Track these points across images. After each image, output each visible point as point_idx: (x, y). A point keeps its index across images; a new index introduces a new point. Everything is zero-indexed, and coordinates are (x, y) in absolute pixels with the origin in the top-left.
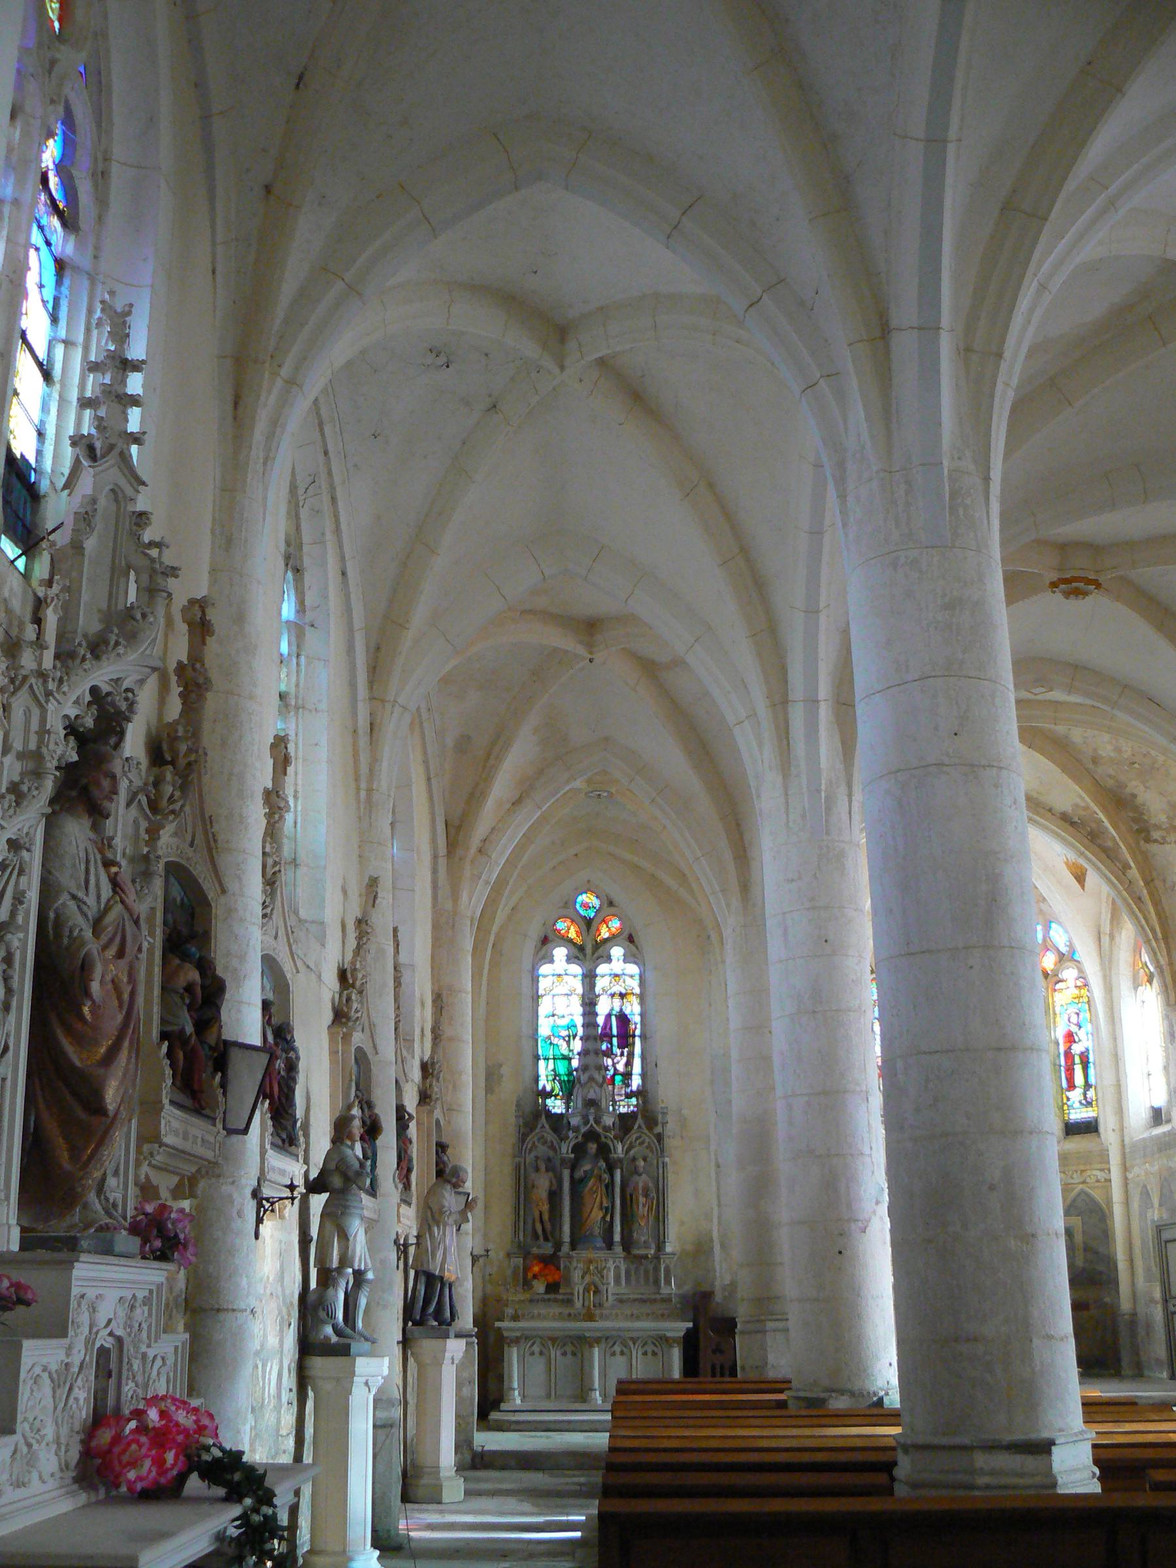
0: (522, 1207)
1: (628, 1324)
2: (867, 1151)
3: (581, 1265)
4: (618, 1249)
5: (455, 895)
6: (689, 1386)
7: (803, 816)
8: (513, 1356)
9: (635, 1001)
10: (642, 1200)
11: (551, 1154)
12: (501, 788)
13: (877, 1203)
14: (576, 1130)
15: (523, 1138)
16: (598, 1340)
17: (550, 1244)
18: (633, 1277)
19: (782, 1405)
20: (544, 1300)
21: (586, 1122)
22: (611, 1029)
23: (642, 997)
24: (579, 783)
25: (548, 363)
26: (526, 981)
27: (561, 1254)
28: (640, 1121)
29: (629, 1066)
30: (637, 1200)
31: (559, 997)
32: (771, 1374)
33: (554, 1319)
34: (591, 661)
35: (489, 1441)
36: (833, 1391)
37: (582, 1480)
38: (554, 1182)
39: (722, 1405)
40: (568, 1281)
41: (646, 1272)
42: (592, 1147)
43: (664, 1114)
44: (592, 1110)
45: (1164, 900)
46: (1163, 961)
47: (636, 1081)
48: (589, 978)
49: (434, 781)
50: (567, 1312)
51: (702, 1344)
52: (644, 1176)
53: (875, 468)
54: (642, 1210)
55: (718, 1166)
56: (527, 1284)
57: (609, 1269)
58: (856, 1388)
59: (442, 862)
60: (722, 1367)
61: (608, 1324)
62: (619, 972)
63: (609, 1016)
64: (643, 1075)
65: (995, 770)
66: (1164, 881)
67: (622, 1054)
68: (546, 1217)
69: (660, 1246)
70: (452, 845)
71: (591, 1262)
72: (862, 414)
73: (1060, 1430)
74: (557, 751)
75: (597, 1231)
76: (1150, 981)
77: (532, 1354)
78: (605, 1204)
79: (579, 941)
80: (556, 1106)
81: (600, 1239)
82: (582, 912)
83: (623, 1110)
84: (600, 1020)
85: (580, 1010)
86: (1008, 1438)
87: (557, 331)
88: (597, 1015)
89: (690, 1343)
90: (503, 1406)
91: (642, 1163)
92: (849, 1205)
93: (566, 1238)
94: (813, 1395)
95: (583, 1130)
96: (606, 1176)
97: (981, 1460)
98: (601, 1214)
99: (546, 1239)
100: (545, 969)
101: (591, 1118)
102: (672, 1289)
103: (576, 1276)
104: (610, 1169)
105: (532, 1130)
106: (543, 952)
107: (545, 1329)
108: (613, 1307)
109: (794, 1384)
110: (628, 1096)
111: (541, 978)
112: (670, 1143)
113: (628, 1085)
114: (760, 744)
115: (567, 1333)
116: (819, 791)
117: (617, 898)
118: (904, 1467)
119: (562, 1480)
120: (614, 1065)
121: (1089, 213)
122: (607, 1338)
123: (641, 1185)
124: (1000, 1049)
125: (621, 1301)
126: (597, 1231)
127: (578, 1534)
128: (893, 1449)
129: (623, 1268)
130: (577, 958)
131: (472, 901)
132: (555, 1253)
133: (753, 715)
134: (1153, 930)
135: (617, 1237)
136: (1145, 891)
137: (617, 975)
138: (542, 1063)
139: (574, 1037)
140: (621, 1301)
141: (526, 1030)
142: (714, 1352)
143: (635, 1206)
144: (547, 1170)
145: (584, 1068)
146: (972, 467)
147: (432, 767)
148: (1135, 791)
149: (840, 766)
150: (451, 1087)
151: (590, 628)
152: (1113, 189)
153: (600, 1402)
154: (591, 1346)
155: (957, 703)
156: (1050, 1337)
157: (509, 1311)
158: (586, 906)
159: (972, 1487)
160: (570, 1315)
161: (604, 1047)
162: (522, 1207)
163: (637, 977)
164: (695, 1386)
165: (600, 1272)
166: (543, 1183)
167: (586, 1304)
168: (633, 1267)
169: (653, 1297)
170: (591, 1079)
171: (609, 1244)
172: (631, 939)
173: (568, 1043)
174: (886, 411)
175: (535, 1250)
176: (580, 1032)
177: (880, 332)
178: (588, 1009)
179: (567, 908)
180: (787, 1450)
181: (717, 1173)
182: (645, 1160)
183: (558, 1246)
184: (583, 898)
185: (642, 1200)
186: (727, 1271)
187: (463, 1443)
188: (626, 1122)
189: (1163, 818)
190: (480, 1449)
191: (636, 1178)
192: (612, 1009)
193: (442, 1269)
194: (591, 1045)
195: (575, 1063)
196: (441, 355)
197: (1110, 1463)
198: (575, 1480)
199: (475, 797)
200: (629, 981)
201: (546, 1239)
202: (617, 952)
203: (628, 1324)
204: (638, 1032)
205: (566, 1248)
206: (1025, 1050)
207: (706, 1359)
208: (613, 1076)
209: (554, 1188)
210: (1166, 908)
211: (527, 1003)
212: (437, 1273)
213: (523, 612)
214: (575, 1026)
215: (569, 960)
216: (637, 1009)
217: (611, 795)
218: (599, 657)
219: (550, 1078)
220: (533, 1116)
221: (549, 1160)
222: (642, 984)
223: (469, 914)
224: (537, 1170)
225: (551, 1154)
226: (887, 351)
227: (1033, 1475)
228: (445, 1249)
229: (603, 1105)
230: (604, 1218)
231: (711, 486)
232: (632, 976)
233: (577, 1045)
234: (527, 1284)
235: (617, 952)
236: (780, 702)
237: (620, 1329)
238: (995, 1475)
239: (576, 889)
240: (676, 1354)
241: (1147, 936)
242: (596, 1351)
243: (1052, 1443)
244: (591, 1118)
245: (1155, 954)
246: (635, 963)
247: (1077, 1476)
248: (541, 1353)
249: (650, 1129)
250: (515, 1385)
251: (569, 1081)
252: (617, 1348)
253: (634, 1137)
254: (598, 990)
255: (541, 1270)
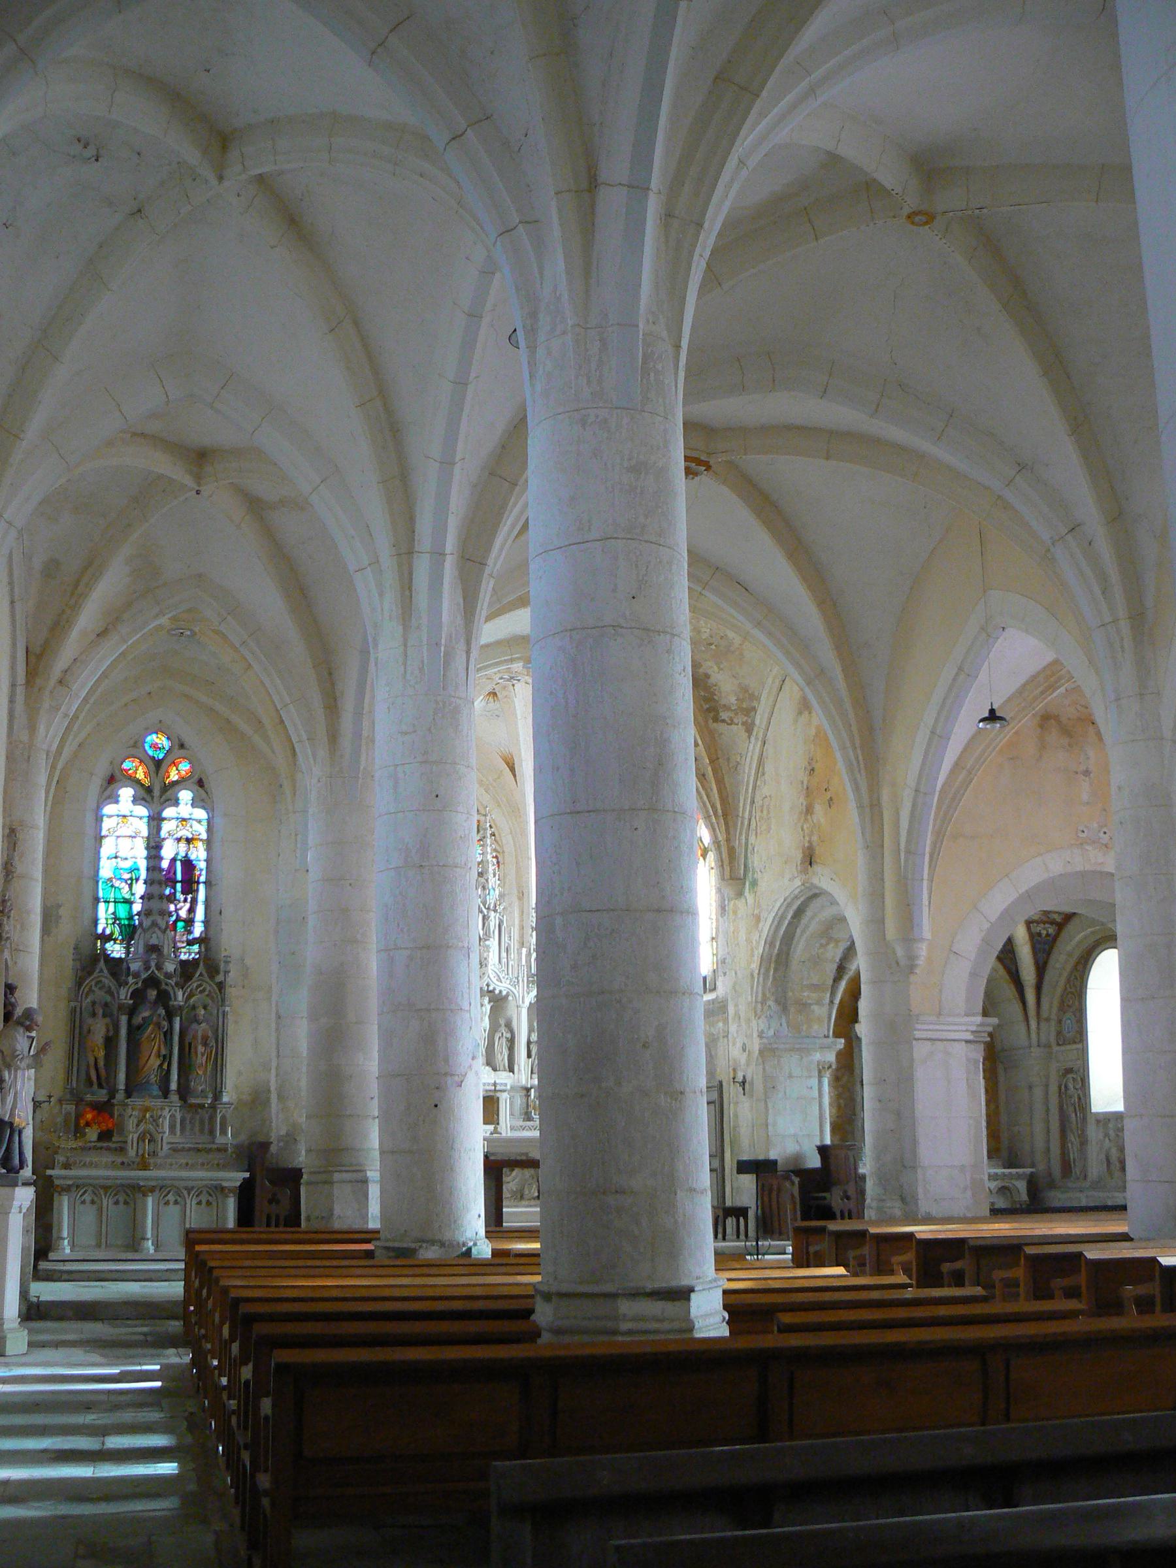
0: (76, 1054)
1: (184, 1174)
2: (465, 1006)
3: (135, 1113)
4: (174, 1098)
5: (32, 728)
6: (244, 1236)
7: (421, 669)
8: (64, 1206)
9: (201, 847)
10: (201, 1049)
11: (108, 998)
12: (87, 619)
13: (473, 1058)
14: (136, 975)
15: (79, 983)
16: (152, 1190)
17: (104, 1092)
18: (188, 1127)
19: (369, 1254)
20: (95, 1148)
21: (147, 968)
22: (175, 873)
23: (209, 843)
24: (164, 620)
25: (208, 173)
26: (90, 818)
27: (115, 1101)
28: (201, 968)
29: (194, 912)
30: (196, 1048)
31: (122, 838)
32: (337, 1225)
33: (106, 1167)
34: (198, 492)
35: (46, 1291)
36: (423, 1241)
37: (145, 1329)
38: (111, 1028)
39: (271, 1255)
40: (121, 1129)
41: (202, 1122)
42: (152, 994)
43: (227, 962)
44: (154, 956)
45: (726, 780)
46: (721, 837)
47: (198, 930)
48: (156, 821)
49: (18, 605)
50: (119, 1160)
51: (258, 1191)
52: (203, 1025)
53: (570, 323)
54: (200, 1059)
55: (279, 1017)
56: (78, 1132)
57: (165, 1118)
58: (446, 1238)
59: (20, 690)
60: (278, 1217)
61: (162, 1173)
62: (186, 815)
63: (173, 860)
64: (206, 922)
65: (668, 636)
66: (728, 759)
67: (185, 900)
68: (101, 1063)
69: (217, 1096)
70: (32, 674)
71: (147, 1109)
72: (562, 265)
73: (698, 1278)
74: (149, 582)
75: (153, 1078)
76: (704, 856)
77: (83, 1202)
78: (163, 1052)
79: (147, 783)
80: (116, 950)
81: (156, 1087)
82: (150, 752)
83: (183, 957)
84: (165, 864)
85: (145, 853)
86: (650, 1286)
87: (221, 139)
88: (162, 858)
89: (246, 1194)
90: (52, 1256)
91: (203, 1012)
92: (446, 1061)
93: (122, 1086)
94: (405, 1245)
95: (144, 976)
96: (165, 1024)
97: (626, 1307)
98: (158, 1062)
99: (100, 1086)
100: (109, 809)
101: (153, 964)
102: (228, 1138)
103: (131, 1124)
104: (170, 1016)
105: (90, 973)
106: (107, 793)
107: (98, 1178)
108: (167, 1156)
109: (382, 1236)
110: (190, 943)
111: (105, 818)
112: (231, 992)
113: (190, 932)
114: (381, 595)
115: (119, 1182)
116: (437, 644)
117: (187, 741)
118: (544, 1314)
119: (123, 1330)
120: (176, 910)
121: (789, 98)
122: (78, 1187)
123: (200, 1034)
124: (659, 911)
125: (175, 1150)
126: (153, 1078)
127: (158, 1384)
128: (532, 1297)
129: (178, 1116)
130: (143, 799)
131: (49, 733)
132: (109, 1100)
133: (376, 561)
134: (713, 806)
135: (174, 1086)
136: (710, 769)
137: (184, 820)
138: (102, 906)
139: (137, 880)
140: (175, 1150)
141: (87, 870)
142: (278, 1202)
143: (193, 1054)
144: (104, 1016)
145: (146, 913)
146: (664, 334)
147: (16, 590)
148: (710, 672)
149: (459, 620)
150: (18, 927)
151: (200, 458)
152: (818, 74)
153: (152, 1251)
154: (145, 1195)
155: (637, 566)
156: (692, 1190)
157: (60, 1158)
158: (155, 746)
159: (615, 1332)
160: (123, 1163)
161: (167, 892)
162: (76, 1054)
163: (205, 823)
164: (250, 1236)
165: (155, 1120)
166: (99, 1029)
167: (140, 1152)
168: (188, 1116)
169: (209, 1146)
170: (154, 924)
171: (166, 1093)
172: (200, 783)
173: (130, 886)
174: (586, 264)
175: (89, 1097)
176: (143, 875)
177: (589, 184)
178: (153, 852)
179: (135, 748)
180: (294, 1300)
181: (277, 1024)
182: (205, 1008)
183: (112, 1093)
184: (152, 738)
185: (201, 1049)
186: (292, 1124)
187: (24, 1294)
188: (187, 969)
189: (733, 699)
190: (35, 1299)
191: (194, 1026)
192: (177, 854)
193: (12, 1115)
194: (155, 889)
195: (137, 907)
196: (90, 146)
197: (739, 1309)
198: (140, 1330)
199: (59, 626)
200: (196, 826)
201: (100, 1086)
202: (185, 796)
203: (184, 1174)
204: (203, 879)
205: (120, 1096)
206: (682, 912)
207: (262, 1207)
208: (175, 922)
209: (111, 1034)
210: (727, 786)
211: (89, 842)
212: (6, 1119)
213: (134, 434)
214: (138, 869)
215: (135, 801)
216: (203, 854)
217: (194, 634)
218: (206, 490)
219: (110, 921)
220: (90, 961)
221: (106, 1005)
222: (209, 830)
223: (45, 747)
224: (94, 1015)
225: (108, 998)
226: (593, 206)
227: (673, 1320)
228: (16, 1093)
229: (165, 951)
230: (161, 1066)
231: (356, 323)
232: (199, 821)
233: (140, 889)
234: (78, 1132)
235: (185, 796)
236: (406, 551)
237: (174, 1179)
238: (637, 1321)
239: (147, 729)
240: (231, 1204)
241: (707, 811)
242: (150, 1201)
243: (692, 1290)
244: (153, 964)
245: (714, 830)
246: (203, 807)
247: (711, 1320)
248: (93, 1202)
249: (212, 977)
250: (65, 1234)
251: (129, 925)
252: (171, 1197)
253: (195, 985)
254: (163, 834)
255: (94, 1118)
